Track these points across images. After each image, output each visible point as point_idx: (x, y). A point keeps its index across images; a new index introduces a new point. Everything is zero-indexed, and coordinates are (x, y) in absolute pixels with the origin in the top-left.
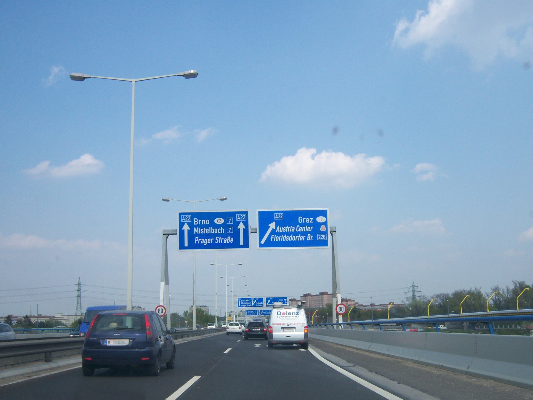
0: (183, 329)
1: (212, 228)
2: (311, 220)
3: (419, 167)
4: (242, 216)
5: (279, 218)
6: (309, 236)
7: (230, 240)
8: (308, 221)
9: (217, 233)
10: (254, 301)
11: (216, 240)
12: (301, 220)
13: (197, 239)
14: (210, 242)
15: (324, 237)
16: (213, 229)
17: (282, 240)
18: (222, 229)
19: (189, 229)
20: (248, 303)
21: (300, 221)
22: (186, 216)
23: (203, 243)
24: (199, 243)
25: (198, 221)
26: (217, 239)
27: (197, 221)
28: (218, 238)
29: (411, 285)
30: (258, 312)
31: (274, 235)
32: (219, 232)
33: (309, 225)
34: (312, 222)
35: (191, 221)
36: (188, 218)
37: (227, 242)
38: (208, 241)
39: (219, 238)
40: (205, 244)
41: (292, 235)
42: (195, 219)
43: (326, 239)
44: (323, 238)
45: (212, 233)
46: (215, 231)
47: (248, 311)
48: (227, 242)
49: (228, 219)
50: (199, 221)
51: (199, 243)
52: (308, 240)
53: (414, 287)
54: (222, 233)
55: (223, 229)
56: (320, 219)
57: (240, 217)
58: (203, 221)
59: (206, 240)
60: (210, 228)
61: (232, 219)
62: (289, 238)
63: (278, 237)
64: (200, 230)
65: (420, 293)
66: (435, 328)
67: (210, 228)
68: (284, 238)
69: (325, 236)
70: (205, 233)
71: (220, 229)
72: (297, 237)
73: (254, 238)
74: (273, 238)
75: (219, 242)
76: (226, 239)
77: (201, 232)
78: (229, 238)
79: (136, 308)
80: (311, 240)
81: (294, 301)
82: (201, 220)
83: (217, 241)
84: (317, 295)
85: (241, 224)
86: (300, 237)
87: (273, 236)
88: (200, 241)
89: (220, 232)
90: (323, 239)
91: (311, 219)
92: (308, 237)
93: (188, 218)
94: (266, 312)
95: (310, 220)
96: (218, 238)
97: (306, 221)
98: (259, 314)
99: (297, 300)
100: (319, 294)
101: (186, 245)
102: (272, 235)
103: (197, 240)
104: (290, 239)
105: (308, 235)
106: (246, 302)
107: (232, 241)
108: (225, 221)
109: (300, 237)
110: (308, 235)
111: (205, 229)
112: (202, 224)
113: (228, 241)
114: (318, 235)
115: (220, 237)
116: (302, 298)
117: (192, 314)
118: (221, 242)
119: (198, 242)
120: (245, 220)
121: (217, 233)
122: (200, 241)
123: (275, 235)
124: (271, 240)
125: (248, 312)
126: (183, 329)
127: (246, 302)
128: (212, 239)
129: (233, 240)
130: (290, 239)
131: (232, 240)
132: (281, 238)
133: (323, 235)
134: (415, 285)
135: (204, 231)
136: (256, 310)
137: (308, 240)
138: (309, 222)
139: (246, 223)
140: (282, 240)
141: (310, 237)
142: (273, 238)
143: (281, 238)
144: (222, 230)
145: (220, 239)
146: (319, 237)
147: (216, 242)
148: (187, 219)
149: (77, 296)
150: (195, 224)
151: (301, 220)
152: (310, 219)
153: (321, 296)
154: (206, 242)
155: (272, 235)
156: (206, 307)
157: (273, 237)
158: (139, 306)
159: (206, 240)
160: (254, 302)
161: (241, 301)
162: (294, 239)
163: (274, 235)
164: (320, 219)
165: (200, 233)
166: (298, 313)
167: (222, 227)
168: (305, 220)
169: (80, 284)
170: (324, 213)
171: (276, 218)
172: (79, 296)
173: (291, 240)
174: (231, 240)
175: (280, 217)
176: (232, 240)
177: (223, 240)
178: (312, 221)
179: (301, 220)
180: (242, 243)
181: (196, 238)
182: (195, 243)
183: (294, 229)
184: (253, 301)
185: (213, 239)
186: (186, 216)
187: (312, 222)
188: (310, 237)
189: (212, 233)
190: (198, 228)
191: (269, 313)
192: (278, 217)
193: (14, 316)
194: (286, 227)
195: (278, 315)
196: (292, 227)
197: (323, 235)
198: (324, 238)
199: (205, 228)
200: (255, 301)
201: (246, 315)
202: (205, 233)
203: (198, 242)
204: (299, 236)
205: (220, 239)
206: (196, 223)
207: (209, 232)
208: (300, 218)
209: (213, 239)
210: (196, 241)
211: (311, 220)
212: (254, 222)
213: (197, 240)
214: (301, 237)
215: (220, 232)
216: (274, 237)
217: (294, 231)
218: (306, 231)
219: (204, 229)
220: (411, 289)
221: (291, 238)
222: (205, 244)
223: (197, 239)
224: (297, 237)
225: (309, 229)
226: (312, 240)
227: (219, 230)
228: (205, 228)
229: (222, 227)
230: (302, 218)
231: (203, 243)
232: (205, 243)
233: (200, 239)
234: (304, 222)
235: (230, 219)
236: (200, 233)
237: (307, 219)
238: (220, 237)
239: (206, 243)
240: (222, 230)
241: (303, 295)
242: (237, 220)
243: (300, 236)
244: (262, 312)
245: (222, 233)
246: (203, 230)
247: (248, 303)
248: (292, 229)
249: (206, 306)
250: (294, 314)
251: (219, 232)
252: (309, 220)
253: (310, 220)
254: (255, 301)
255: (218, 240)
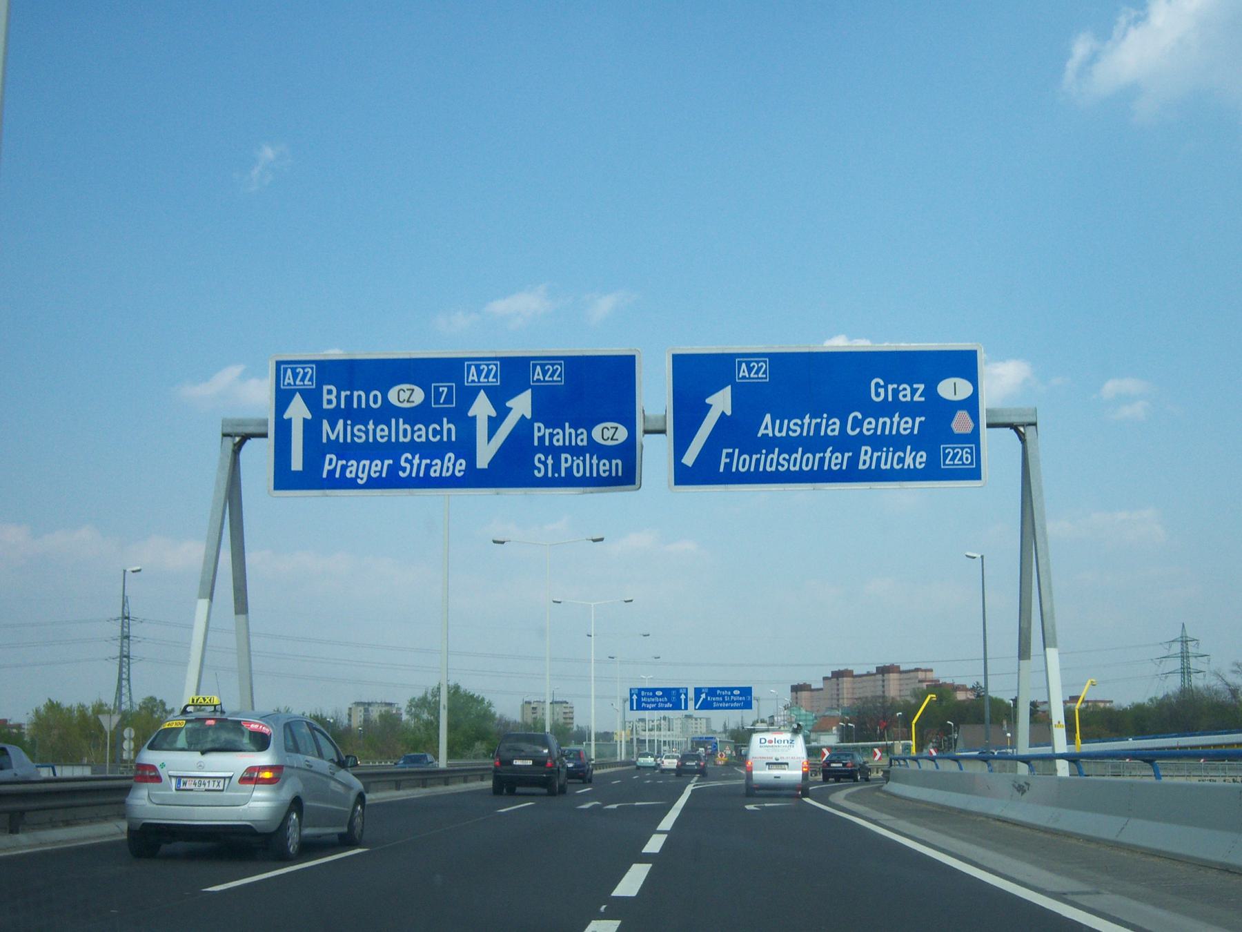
0: (65, 772)
1: (401, 421)
2: (919, 392)
3: (1111, 387)
4: (754, 366)
5: (547, 379)
6: (866, 452)
7: (454, 465)
8: (905, 396)
9: (423, 439)
10: (499, 398)
11: (403, 464)
12: (882, 391)
13: (643, 705)
14: (378, 474)
15: (965, 456)
16: (408, 427)
17: (761, 469)
18: (446, 426)
19: (729, 413)
20: (422, 433)
21: (878, 395)
22: (752, 361)
23: (353, 475)
24: (337, 475)
25: (338, 397)
26: (407, 460)
27: (333, 397)
28: (409, 456)
29: (1178, 635)
30: (683, 697)
31: (731, 450)
32: (434, 436)
33: (909, 410)
34: (923, 399)
35: (768, 380)
36: (554, 372)
37: (443, 475)
38: (373, 468)
39: (414, 458)
40: (362, 479)
41: (800, 450)
42: (325, 388)
43: (971, 463)
44: (961, 459)
45: (401, 439)
46: (413, 432)
47: (640, 690)
48: (443, 475)
49: (437, 388)
50: (343, 394)
51: (337, 475)
52: (861, 467)
53: (1184, 641)
54: (445, 439)
55: (452, 426)
56: (952, 389)
57: (545, 373)
58: (356, 394)
59: (364, 466)
60: (393, 421)
61: (450, 388)
62: (788, 461)
63: (747, 457)
64: (349, 428)
65: (1203, 677)
66: (348, 787)
67: (393, 421)
68: (772, 459)
69: (971, 454)
70: (371, 440)
71: (438, 428)
72: (818, 456)
73: (691, 704)
74: (728, 460)
75: (414, 475)
76: (438, 461)
77: (353, 435)
78: (450, 458)
79: (377, 705)
80: (550, 475)
81: (805, 691)
82: (348, 393)
83: (404, 470)
84: (869, 674)
85: (683, 695)
86: (830, 458)
87: (728, 455)
88: (344, 468)
89: (438, 437)
90: (963, 464)
91: (918, 389)
92: (862, 457)
93: (554, 372)
94: (723, 697)
95: (914, 391)
96: (409, 456)
97: (901, 395)
98: (691, 704)
99: (812, 687)
100: (875, 671)
101: (635, 708)
102: (725, 451)
103: (330, 463)
104: (794, 465)
105: (864, 448)
106: (387, 413)
107: (460, 471)
108: (385, 398)
109: (830, 458)
110: (864, 448)
111: (371, 426)
112: (355, 406)
113: (448, 471)
114: (945, 449)
115: (417, 456)
116: (826, 681)
117: (433, 726)
118: (421, 474)
119: (334, 471)
120: (766, 378)
121: (423, 439)
122: (344, 468)
123: (737, 451)
124: (721, 470)
125: (639, 695)
126: (65, 772)
127: (387, 413)
128: (387, 462)
129: (463, 467)
130: (794, 465)
131: (461, 464)
132: (758, 461)
133: (962, 449)
134: (1190, 634)
135: (367, 433)
136: (677, 690)
137: (861, 467)
138: (908, 399)
139: (686, 694)
140: (761, 469)
141: (871, 458)
142: (728, 460)
143: (758, 461)
144: (449, 430)
145: (416, 461)
146: (946, 456)
147: (401, 474)
148: (755, 373)
149: (119, 654)
150: (325, 406)
151: (882, 391)
152: (915, 386)
153: (880, 676)
154: (363, 472)
155: (725, 451)
156: (565, 705)
157: (726, 457)
158: (387, 701)
159: (364, 466)
160: (503, 412)
161: (312, 399)
162: (807, 465)
163: (731, 450)
164: (952, 389)
165: (349, 440)
166: (793, 741)
167: (445, 420)
168: (896, 392)
169: (128, 618)
170: (965, 364)
171: (536, 377)
172: (125, 657)
173: (797, 468)
174: (458, 467)
175: (552, 376)
176: (921, 457)
177: (428, 467)
178: (920, 396)
179: (878, 390)
180: (683, 708)
181: (328, 457)
182: (325, 475)
183: (837, 427)
184: (482, 408)
185: (391, 462)
186: (752, 361)
187: (923, 399)
188: (871, 458)
189: (401, 439)
190: (341, 422)
191: (733, 702)
192: (749, 374)
193: (11, 723)
194: (802, 419)
195: (760, 742)
196: (828, 420)
197: (962, 449)
198: (967, 459)
199: (371, 422)
200: (521, 405)
201: (632, 709)
202: (371, 440)
203: (334, 471)
204: (828, 455)
205: (416, 461)
206: (330, 402)
207: (390, 436)
208: (877, 385)
209: (391, 462)
210: (327, 467)
211: (919, 392)
212: (691, 694)
213: (330, 463)
214: (837, 458)
215: (438, 437)
216: (730, 456)
217: (836, 433)
218: (894, 432)
219: (366, 425)
220: (1177, 648)
221: (796, 459)
222: (362, 479)
223: (331, 460)
224: (818, 456)
225: (906, 425)
226: (553, 474)
227: (434, 429)
228: (371, 422)
229: (445, 420)
230: (882, 383)
231: (353, 475)
232: (360, 474)
233: (428, 461)
234: (890, 399)
235: (446, 389)
236: (349, 440)
237: (901, 388)
238: (417, 456)
239: (365, 476)
240: (449, 430)
241: (830, 675)
242: (739, 379)
243: (832, 452)
244: (703, 696)
245: (445, 439)
246: (363, 428)
247: (422, 433)
248: (827, 426)
249: (567, 703)
250: (786, 742)
251: (434, 436)
252: (908, 392)
253: (914, 391)
254: (521, 405)
255: (408, 466)
